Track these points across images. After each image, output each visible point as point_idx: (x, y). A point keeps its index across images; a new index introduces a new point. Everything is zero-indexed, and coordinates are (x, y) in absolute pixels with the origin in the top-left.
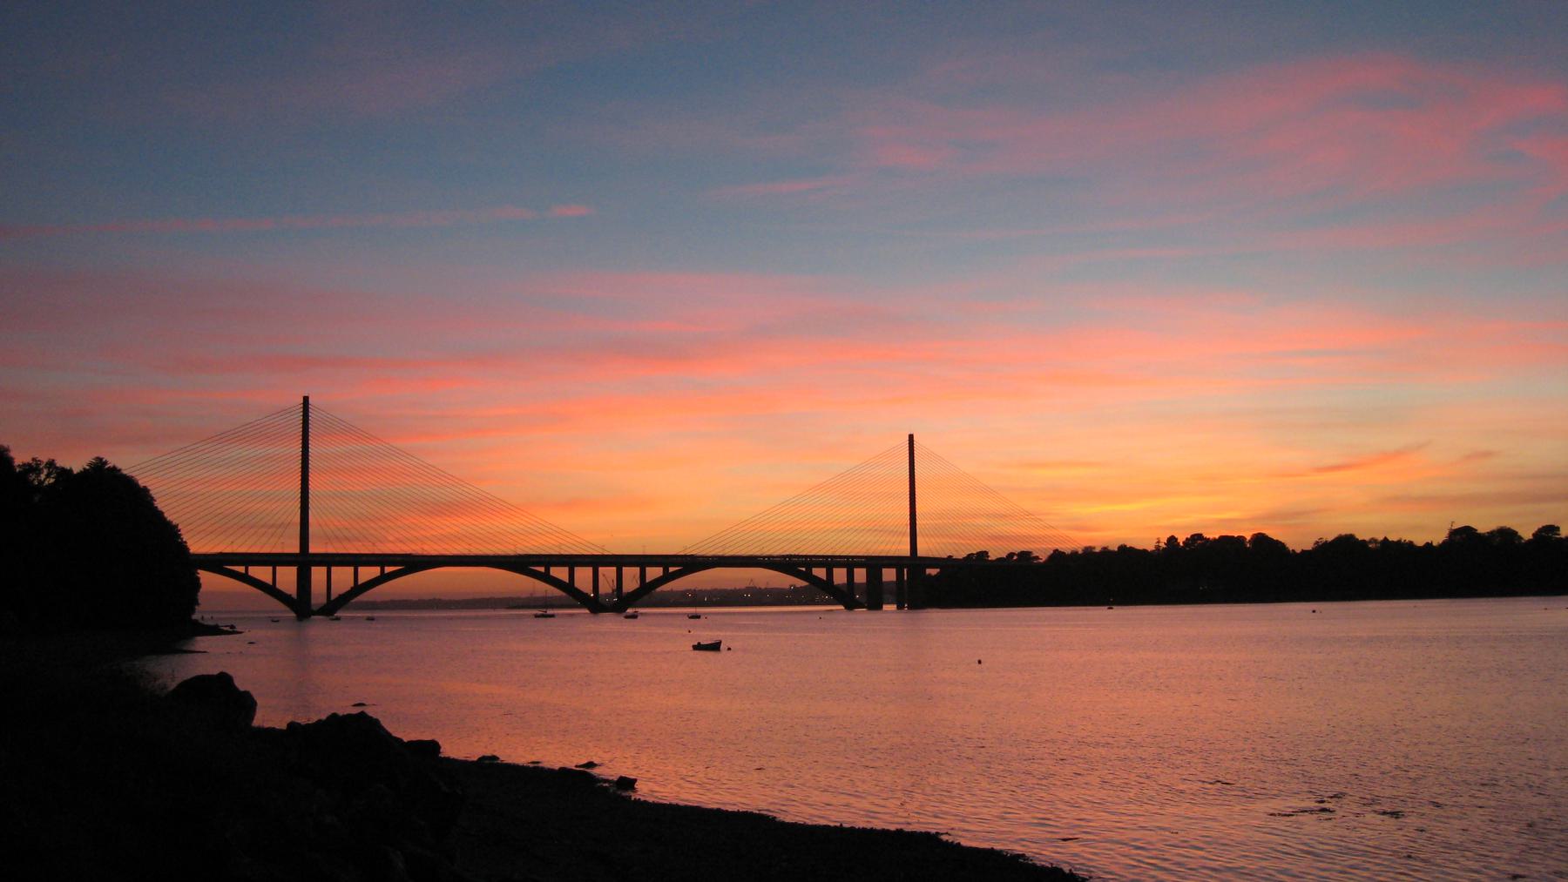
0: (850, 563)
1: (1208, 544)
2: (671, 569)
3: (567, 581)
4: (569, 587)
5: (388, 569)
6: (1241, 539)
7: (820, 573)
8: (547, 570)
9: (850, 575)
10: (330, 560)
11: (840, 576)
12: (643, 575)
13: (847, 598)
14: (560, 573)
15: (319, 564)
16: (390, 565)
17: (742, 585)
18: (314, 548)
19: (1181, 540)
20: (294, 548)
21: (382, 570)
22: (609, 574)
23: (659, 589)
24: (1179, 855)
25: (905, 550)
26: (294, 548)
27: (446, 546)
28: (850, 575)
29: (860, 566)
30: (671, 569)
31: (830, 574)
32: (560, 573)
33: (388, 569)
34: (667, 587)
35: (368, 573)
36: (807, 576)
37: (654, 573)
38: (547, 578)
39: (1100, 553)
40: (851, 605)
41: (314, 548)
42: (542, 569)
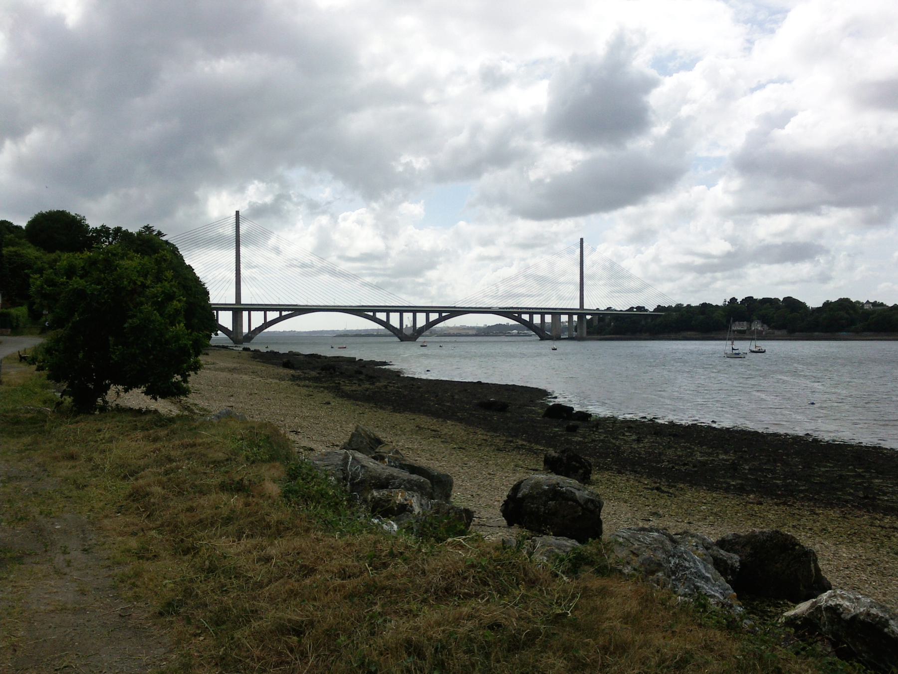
0: (543, 312)
1: (203, 304)
2: (444, 314)
3: (528, 320)
4: (386, 324)
5: (284, 313)
6: (777, 300)
7: (526, 317)
8: (374, 314)
9: (543, 319)
10: (251, 308)
11: (537, 319)
12: (428, 318)
13: (542, 333)
14: (382, 316)
15: (245, 309)
16: (285, 310)
17: (481, 325)
18: (244, 301)
19: (739, 300)
20: (232, 301)
21: (281, 314)
22: (408, 317)
23: (266, 330)
24: (310, 650)
25: (577, 306)
26: (232, 301)
27: (404, 296)
28: (543, 319)
29: (575, 314)
30: (444, 314)
31: (531, 318)
32: (382, 316)
33: (284, 313)
34: (441, 325)
35: (272, 315)
36: (519, 319)
37: (434, 316)
38: (374, 319)
39: (675, 307)
40: (543, 337)
41: (244, 301)
42: (371, 314)
